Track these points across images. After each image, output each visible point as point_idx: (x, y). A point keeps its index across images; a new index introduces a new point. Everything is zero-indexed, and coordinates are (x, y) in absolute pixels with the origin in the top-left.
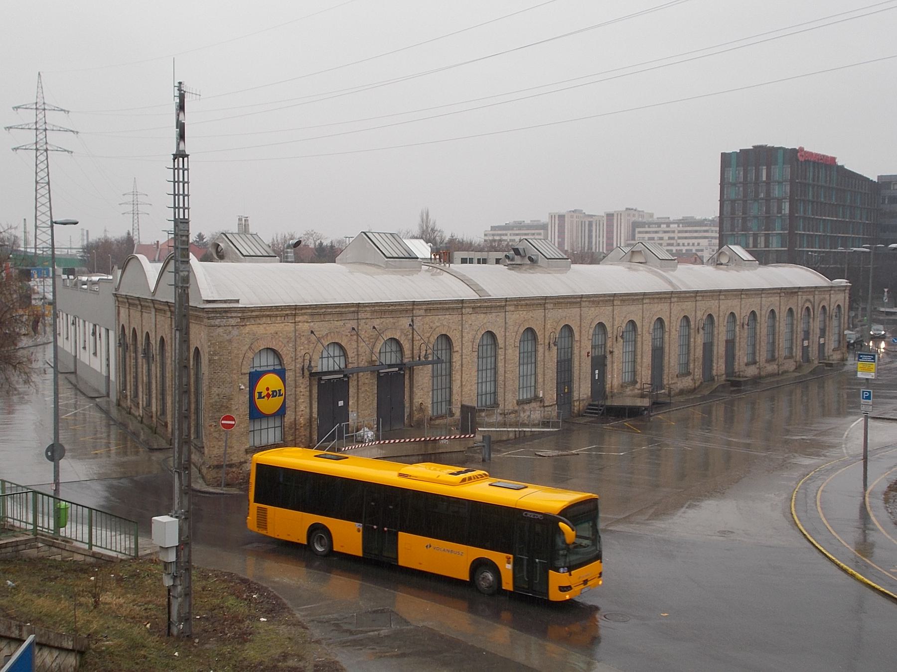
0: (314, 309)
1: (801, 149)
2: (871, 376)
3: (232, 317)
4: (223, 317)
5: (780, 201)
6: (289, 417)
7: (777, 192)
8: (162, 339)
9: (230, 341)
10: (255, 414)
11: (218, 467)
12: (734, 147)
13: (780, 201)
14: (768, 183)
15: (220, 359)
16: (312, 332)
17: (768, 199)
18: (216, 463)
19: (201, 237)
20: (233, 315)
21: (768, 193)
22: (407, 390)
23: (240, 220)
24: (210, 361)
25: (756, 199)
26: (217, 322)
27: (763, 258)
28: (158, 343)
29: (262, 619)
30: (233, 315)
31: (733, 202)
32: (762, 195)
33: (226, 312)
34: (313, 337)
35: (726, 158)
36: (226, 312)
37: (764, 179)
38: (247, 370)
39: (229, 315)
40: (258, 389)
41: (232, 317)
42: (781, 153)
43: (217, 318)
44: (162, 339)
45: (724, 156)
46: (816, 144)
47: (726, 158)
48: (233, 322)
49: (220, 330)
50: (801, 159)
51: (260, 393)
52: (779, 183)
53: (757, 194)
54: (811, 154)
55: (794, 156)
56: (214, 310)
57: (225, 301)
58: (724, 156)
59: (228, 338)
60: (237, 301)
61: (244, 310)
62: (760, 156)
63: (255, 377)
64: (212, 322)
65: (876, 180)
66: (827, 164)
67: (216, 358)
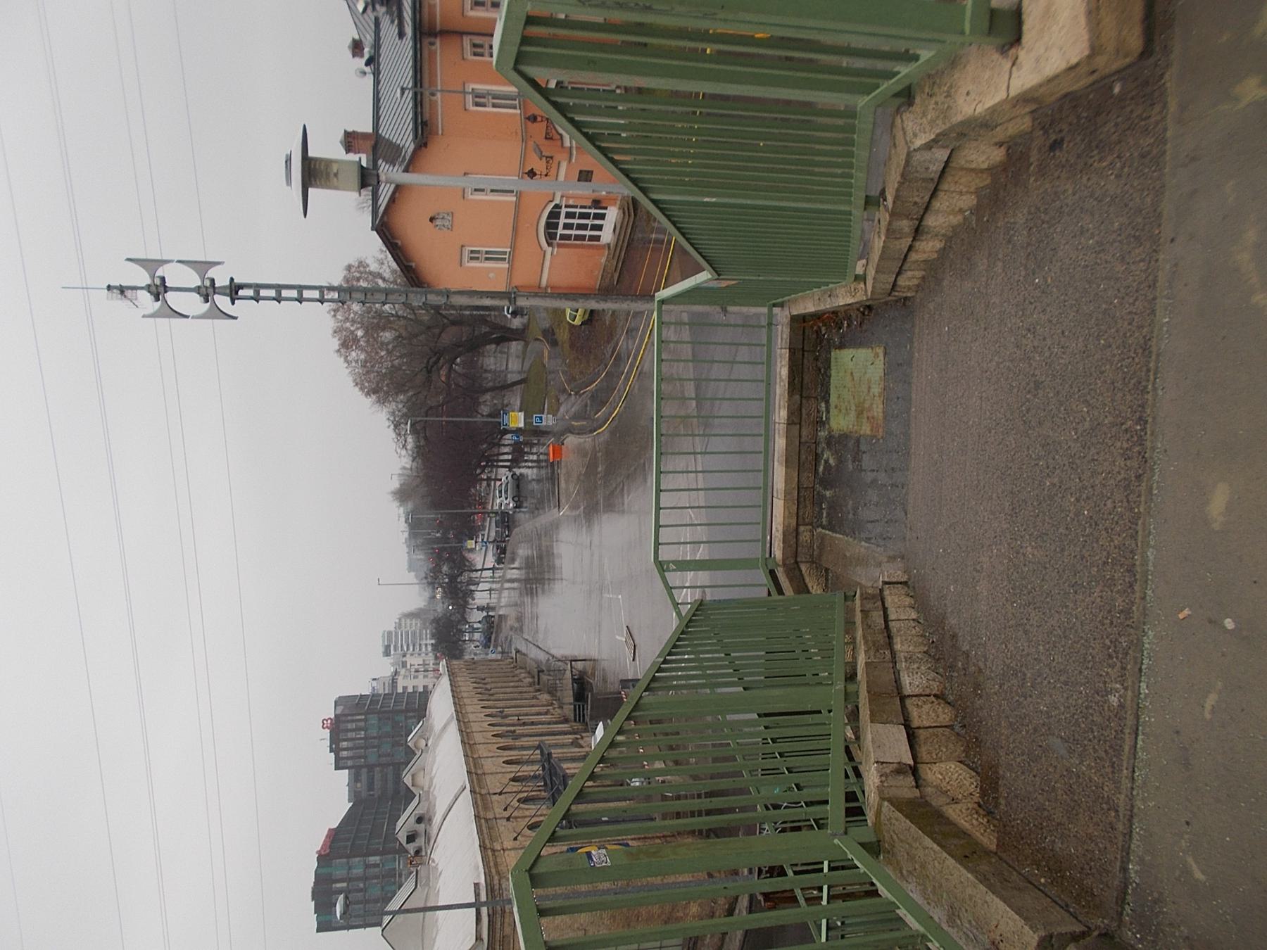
1: (318, 852)
2: (521, 415)
5: (367, 866)
7: (358, 871)
8: (514, 779)
12: (313, 920)
13: (367, 866)
14: (349, 880)
17: (365, 878)
19: (405, 688)
20: (496, 881)
21: (358, 879)
25: (364, 890)
29: (1186, 612)
32: (361, 885)
33: (492, 890)
35: (324, 926)
36: (492, 890)
37: (345, 885)
39: (497, 887)
44: (514, 779)
45: (320, 929)
46: (318, 841)
52: (350, 868)
53: (361, 890)
55: (323, 859)
60: (476, 885)
61: (488, 874)
62: (322, 895)
66: (335, 837)
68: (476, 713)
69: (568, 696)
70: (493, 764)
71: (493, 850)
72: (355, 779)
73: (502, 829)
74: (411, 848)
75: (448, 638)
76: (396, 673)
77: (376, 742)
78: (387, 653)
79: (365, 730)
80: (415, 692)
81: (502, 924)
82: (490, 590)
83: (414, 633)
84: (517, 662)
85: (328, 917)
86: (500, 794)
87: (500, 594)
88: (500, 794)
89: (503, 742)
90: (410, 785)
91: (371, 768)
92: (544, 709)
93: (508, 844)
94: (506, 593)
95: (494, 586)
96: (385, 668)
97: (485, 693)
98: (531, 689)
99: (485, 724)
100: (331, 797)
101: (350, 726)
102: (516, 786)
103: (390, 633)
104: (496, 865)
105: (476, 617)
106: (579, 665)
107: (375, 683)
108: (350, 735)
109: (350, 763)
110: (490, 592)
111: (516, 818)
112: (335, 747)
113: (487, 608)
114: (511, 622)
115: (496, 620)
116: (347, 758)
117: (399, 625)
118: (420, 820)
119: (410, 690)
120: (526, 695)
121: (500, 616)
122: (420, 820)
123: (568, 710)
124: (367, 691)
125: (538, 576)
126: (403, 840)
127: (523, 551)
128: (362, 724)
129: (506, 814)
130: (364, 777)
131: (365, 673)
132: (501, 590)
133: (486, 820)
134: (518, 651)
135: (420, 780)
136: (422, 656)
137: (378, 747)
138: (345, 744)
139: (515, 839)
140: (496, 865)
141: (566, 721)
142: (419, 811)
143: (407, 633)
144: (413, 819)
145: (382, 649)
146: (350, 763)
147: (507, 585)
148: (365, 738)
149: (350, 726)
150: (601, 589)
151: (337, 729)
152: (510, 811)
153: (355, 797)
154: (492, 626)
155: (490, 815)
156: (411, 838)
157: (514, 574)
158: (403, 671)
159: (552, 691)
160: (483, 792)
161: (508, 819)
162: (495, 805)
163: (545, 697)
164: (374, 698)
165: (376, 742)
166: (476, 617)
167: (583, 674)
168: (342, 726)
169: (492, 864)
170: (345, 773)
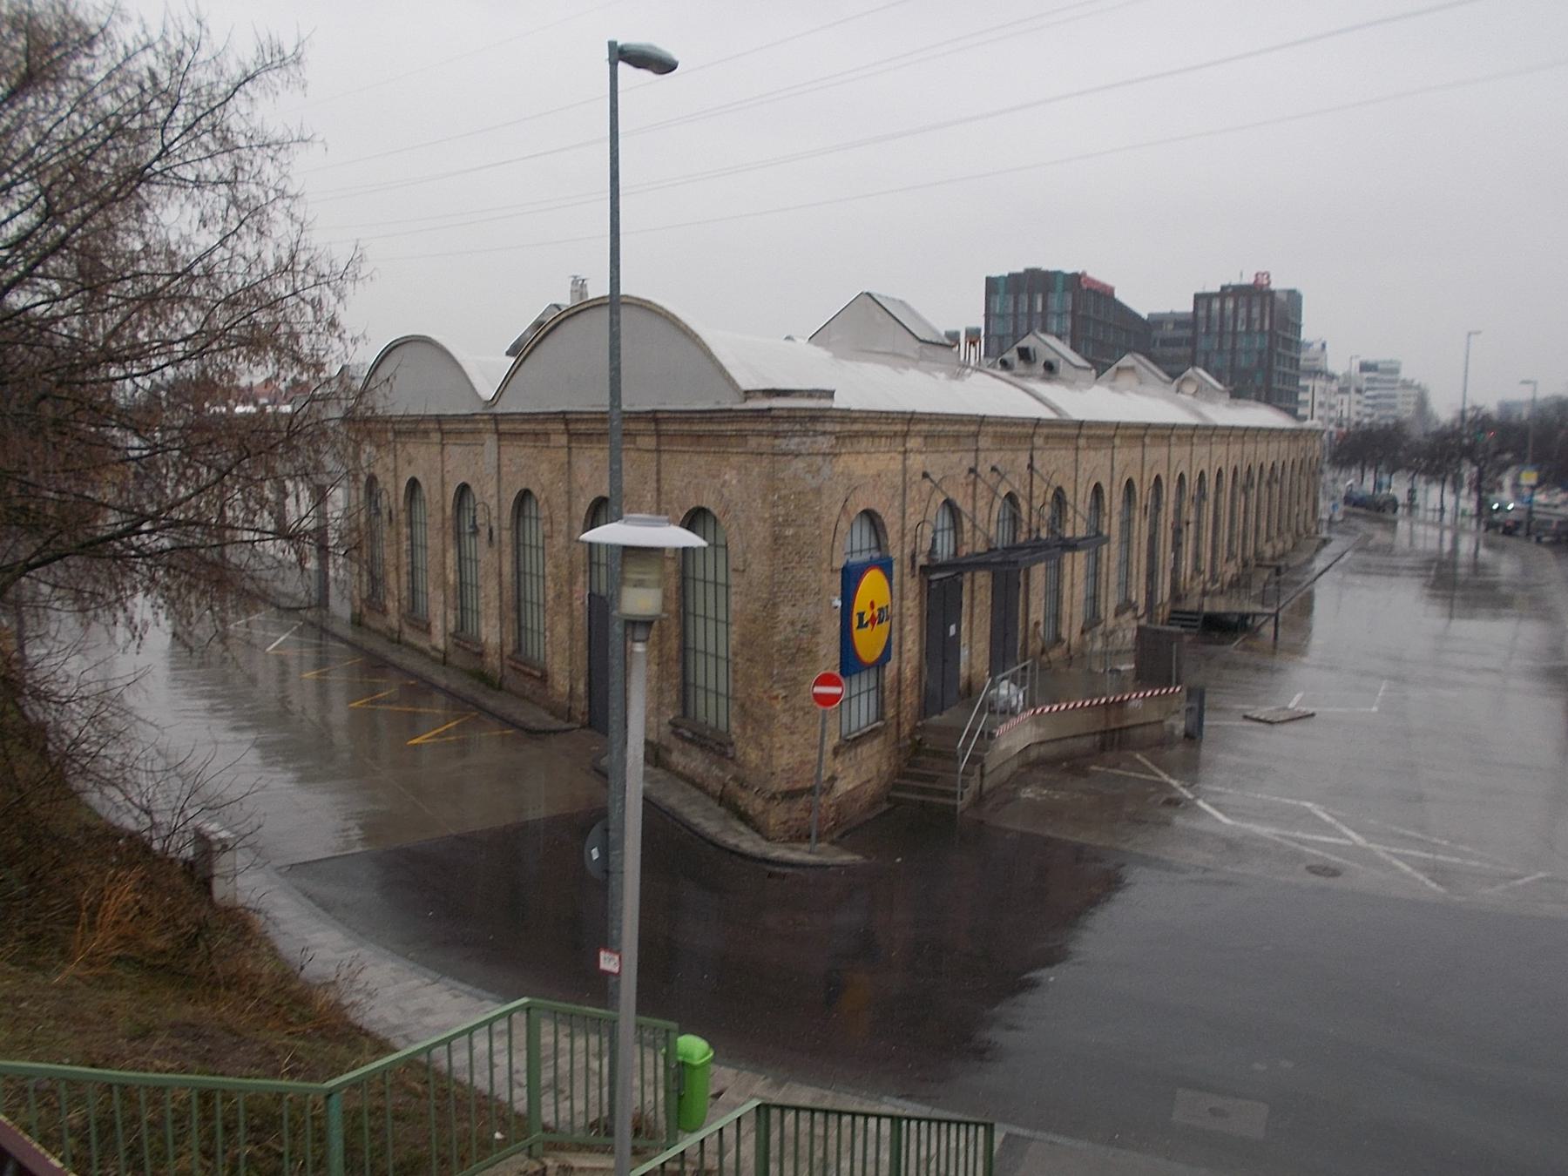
0: (1006, 424)
1: (1084, 274)
3: (824, 433)
4: (805, 434)
6: (891, 668)
8: (1059, 495)
9: (818, 491)
10: (850, 662)
11: (791, 795)
12: (1001, 270)
15: (796, 535)
16: (925, 475)
18: (785, 787)
20: (829, 427)
22: (1021, 596)
23: (575, 282)
24: (776, 540)
26: (793, 444)
27: (1237, 394)
28: (402, 492)
30: (829, 427)
31: (1001, 338)
34: (928, 484)
35: (992, 285)
37: (1039, 309)
38: (839, 564)
39: (819, 427)
40: (857, 609)
41: (824, 433)
42: (1060, 280)
43: (794, 434)
45: (991, 282)
46: (1099, 272)
47: (992, 285)
48: (824, 444)
49: (800, 464)
50: (1085, 286)
51: (861, 615)
52: (1060, 315)
54: (1093, 281)
55: (1075, 280)
56: (792, 416)
57: (810, 394)
58: (991, 282)
59: (814, 483)
60: (830, 394)
61: (847, 416)
63: (850, 578)
64: (782, 444)
65: (1145, 316)
67: (789, 532)
68: (1208, 459)
69: (1220, 606)
70: (1095, 464)
71: (906, 435)
72: (1179, 321)
73: (955, 457)
74: (1012, 355)
75: (1372, 446)
76: (1331, 377)
77: (1228, 346)
78: (1365, 367)
79: (1249, 332)
80: (1298, 402)
81: (760, 434)
82: (1442, 510)
83: (1393, 407)
84: (1308, 539)
85: (1002, 291)
86: (1031, 467)
87: (1433, 524)
88: (1031, 467)
89: (1143, 492)
90: (1121, 363)
91: (1192, 342)
92: (1206, 564)
93: (916, 462)
94: (1433, 533)
95: (1447, 517)
96: (1339, 362)
97: (1245, 481)
98: (1250, 552)
99: (1183, 468)
100: (1154, 289)
101: (1256, 312)
102: (1043, 494)
103: (1396, 371)
104: (872, 434)
105: (1399, 488)
106: (1268, 630)
107: (1317, 346)
108: (1242, 312)
109: (1202, 313)
110: (1436, 513)
111: (975, 484)
112: (1226, 292)
113: (1411, 505)
114: (1380, 536)
115: (1389, 516)
116: (1209, 309)
117: (1407, 385)
118: (1049, 367)
119: (1302, 396)
120: (1237, 543)
121: (1395, 523)
122: (1049, 367)
123: (1191, 604)
124: (1306, 335)
125: (1453, 584)
126: (1023, 343)
127: (1506, 566)
128: (1257, 326)
129: (984, 469)
130: (1181, 333)
131: (1335, 333)
132: (1440, 525)
133: (976, 435)
134: (1325, 542)
135: (1125, 380)
136: (1353, 410)
137: (1220, 350)
138: (1230, 304)
139: (925, 475)
140: (872, 434)
141: (1176, 595)
142: (1062, 366)
143: (1394, 397)
144: (1051, 356)
145: (1370, 358)
146: (1202, 313)
147: (1448, 535)
148: (1235, 333)
149: (1256, 312)
150: (1399, 679)
151: (1254, 294)
152: (992, 479)
153: (1157, 322)
154: (1378, 509)
155: (984, 442)
156: (1025, 354)
157: (1466, 545)
158: (1334, 387)
159: (1238, 584)
160: (1039, 441)
161: (972, 470)
162: (1009, 456)
163: (1230, 570)
164: (1294, 343)
165: (1228, 346)
166: (1399, 488)
167: (1254, 632)
168: (1256, 301)
169: (874, 427)
170: (1188, 307)
